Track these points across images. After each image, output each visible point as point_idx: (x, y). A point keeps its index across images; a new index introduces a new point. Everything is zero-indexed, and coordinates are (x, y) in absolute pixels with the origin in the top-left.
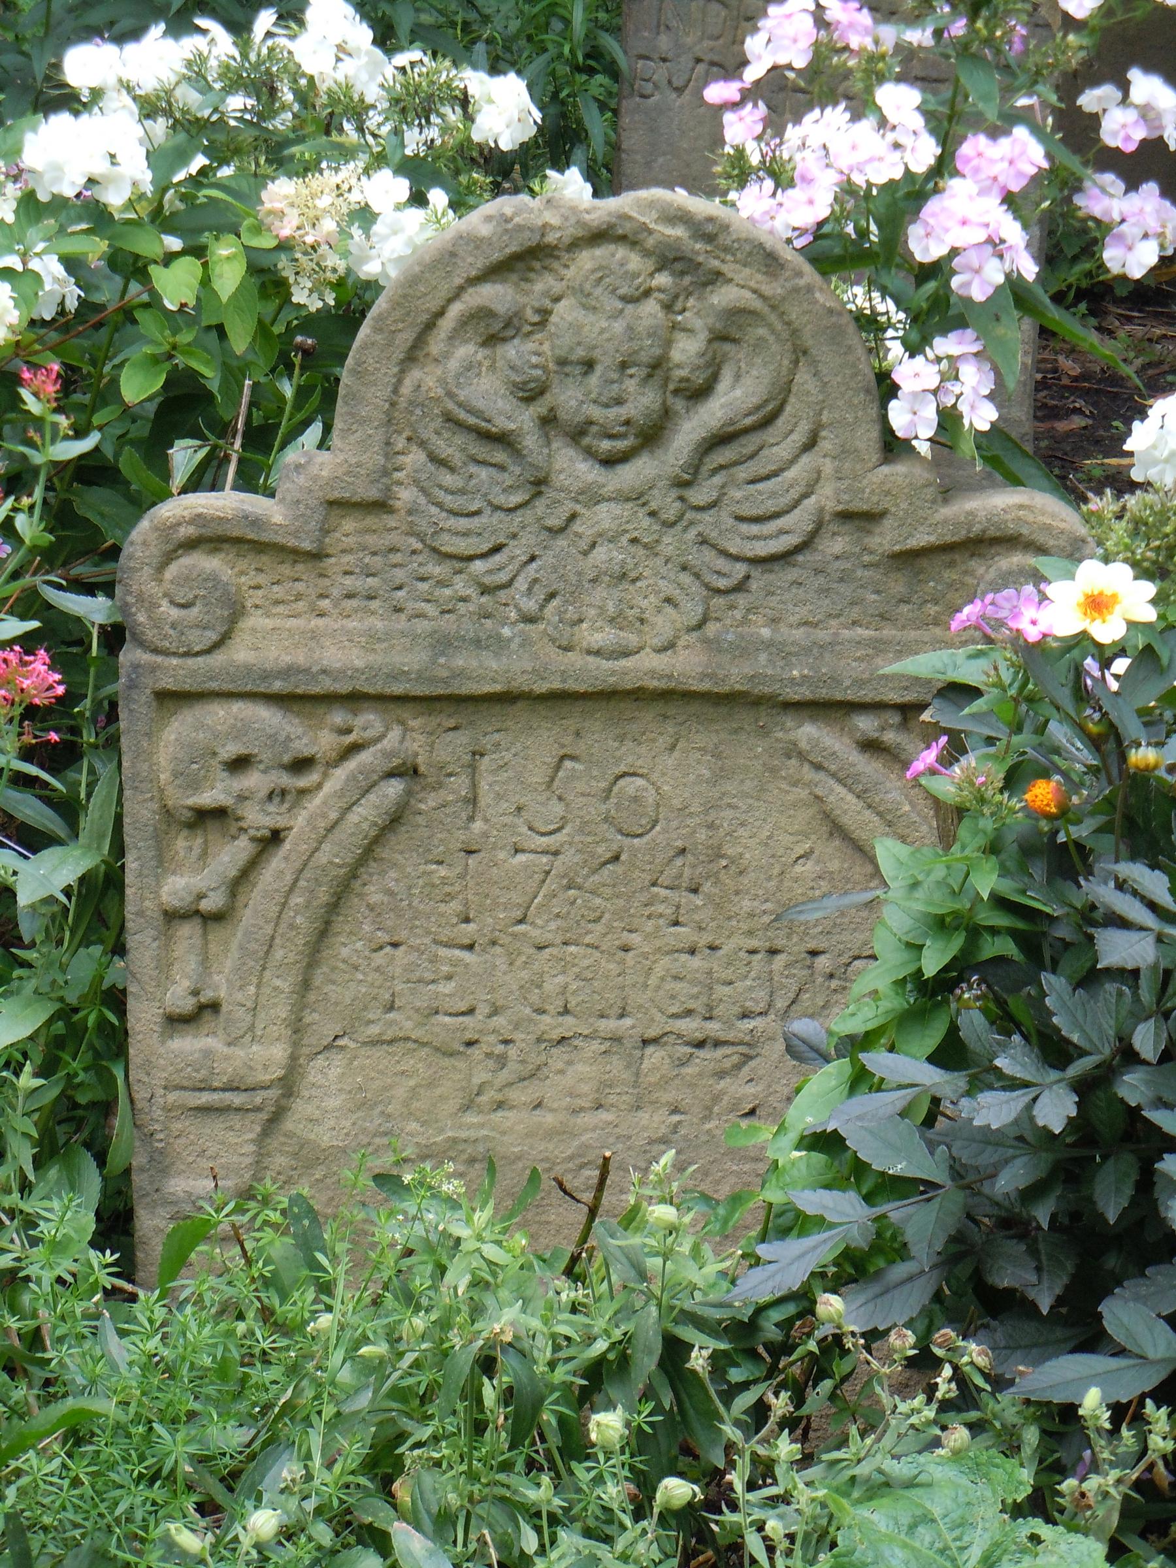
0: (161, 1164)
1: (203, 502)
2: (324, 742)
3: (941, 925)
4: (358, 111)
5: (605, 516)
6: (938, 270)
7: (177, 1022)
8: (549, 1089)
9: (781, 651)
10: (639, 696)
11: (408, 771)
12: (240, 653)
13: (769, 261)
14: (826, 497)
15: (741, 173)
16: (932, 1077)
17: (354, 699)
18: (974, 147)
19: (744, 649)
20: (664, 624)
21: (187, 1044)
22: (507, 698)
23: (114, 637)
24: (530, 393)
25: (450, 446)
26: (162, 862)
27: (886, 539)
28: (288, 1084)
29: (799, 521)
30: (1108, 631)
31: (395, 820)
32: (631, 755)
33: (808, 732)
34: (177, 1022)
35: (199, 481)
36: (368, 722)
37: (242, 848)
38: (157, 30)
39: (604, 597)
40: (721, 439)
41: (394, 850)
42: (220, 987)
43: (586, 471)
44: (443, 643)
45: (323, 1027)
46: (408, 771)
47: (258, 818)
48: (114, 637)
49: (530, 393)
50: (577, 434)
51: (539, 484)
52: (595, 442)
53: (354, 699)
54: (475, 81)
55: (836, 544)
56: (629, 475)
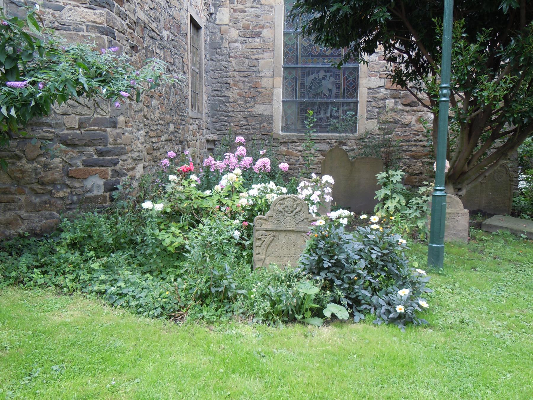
0: (255, 265)
1: (260, 216)
2: (268, 234)
3: (310, 245)
4: (274, 190)
5: (289, 218)
6: (313, 201)
7: (257, 254)
8: (284, 260)
9: (301, 228)
10: (291, 231)
11: (274, 236)
12: (262, 227)
13: (301, 200)
14: (305, 217)
15: (299, 194)
16: (309, 256)
17: (270, 231)
18: (315, 192)
19: (298, 228)
20: (293, 226)
21: (257, 256)
22: (281, 231)
23: (253, 226)
24: (283, 209)
25: (278, 212)
26: (256, 242)
27: (309, 220)
28: (265, 259)
29: (303, 218)
30: (321, 225)
31: (273, 240)
32: (290, 235)
33: (303, 234)
34: (257, 254)
35: (260, 215)
36: (271, 232)
37: (261, 242)
38: (341, 209)
39: (288, 224)
40: (297, 212)
41: (273, 242)
42: (260, 252)
43: (287, 214)
44: (277, 227)
45: (267, 255)
46: (274, 236)
47: (263, 239)
48: (253, 226)
49: (283, 209)
50: (287, 212)
51: (284, 215)
52: (205, 111)
53: (270, 231)
54: (282, 188)
55: (305, 220)
56: (290, 215)
